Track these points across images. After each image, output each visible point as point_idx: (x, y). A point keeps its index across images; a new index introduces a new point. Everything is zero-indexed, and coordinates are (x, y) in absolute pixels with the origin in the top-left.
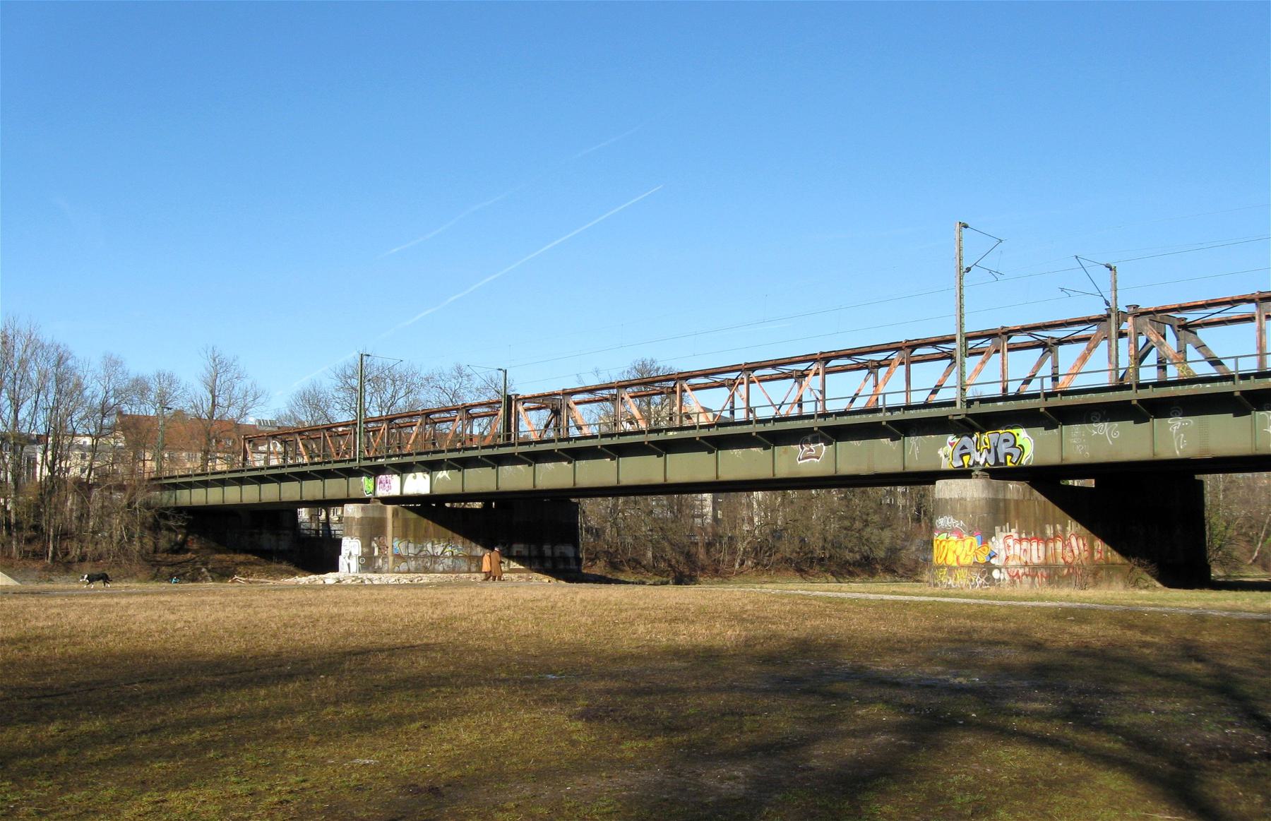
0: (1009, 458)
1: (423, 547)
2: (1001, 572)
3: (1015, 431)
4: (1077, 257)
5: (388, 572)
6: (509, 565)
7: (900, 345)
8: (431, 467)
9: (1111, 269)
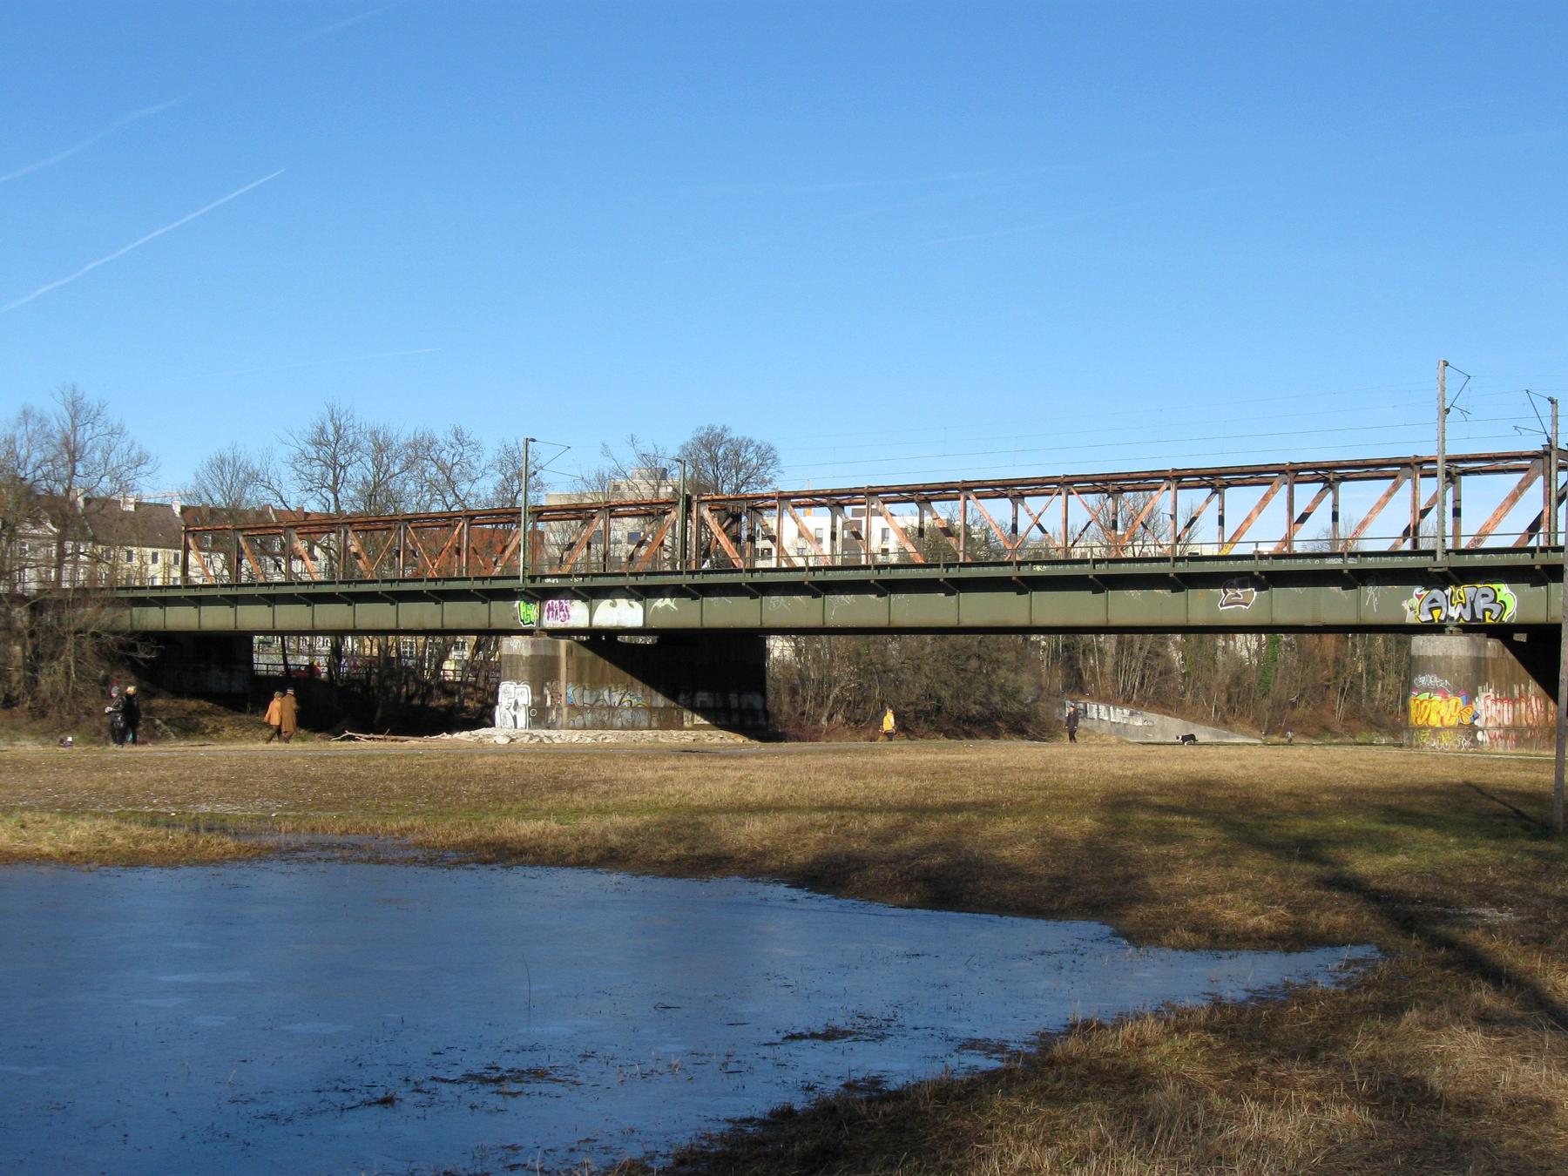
0: (1488, 614)
1: (599, 695)
3: (1495, 586)
4: (1527, 391)
5: (562, 728)
6: (693, 719)
7: (1282, 468)
8: (643, 593)
9: (1552, 402)
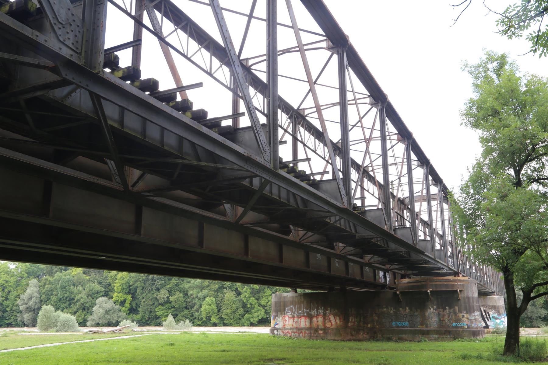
2: (278, 331)
